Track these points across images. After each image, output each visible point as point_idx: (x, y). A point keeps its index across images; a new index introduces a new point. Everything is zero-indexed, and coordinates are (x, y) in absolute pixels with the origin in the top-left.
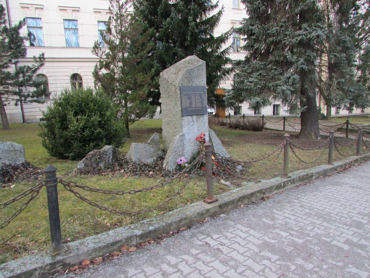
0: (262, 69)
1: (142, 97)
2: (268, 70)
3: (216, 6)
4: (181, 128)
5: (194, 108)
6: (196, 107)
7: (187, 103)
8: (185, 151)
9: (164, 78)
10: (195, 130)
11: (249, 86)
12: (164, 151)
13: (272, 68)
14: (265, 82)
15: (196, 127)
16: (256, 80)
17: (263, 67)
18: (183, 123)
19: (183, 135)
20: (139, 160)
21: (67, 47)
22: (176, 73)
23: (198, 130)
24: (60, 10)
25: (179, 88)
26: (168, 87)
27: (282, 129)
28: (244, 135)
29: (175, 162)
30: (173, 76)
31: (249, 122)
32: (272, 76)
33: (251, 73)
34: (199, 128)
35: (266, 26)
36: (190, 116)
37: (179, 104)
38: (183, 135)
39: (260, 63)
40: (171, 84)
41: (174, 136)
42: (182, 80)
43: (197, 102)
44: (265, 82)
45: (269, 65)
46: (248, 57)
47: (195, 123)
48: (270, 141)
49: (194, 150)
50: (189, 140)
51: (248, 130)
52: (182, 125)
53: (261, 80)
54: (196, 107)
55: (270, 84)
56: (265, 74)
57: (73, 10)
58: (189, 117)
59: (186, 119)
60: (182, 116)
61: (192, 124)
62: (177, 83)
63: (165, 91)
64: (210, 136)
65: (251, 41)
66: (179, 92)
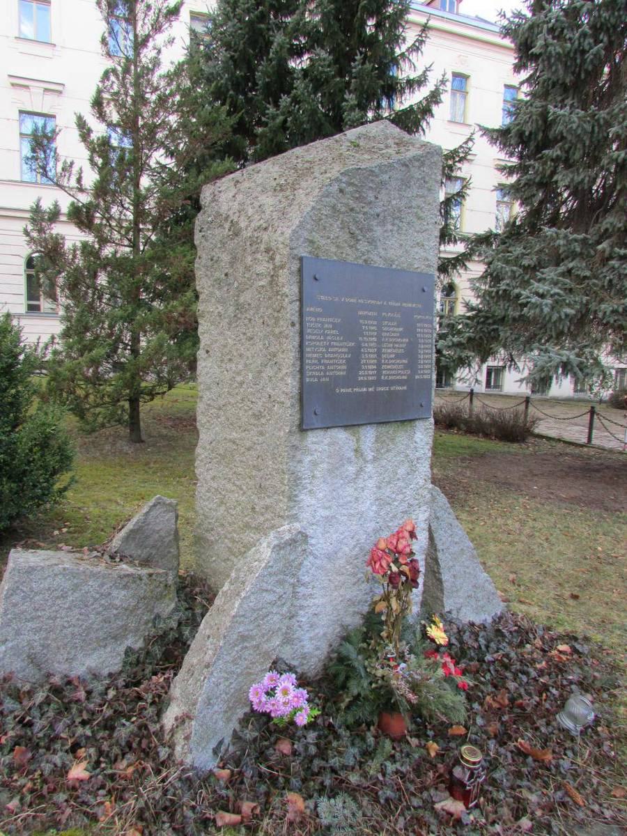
0: (573, 255)
1: (177, 322)
2: (597, 259)
3: (420, 82)
4: (292, 498)
5: (368, 384)
6: (378, 382)
7: (331, 357)
8: (303, 617)
9: (218, 214)
10: (367, 505)
11: (535, 306)
12: (195, 595)
13: (612, 251)
14: (585, 299)
15: (371, 484)
16: (556, 290)
17: (578, 250)
18: (304, 470)
19: (301, 539)
20: (33, 659)
21: (22, 182)
22: (282, 188)
23: (382, 502)
24: (13, 85)
25: (295, 266)
26: (234, 260)
27: (584, 440)
28: (483, 456)
29: (240, 697)
30: (268, 201)
31: (488, 414)
32: (610, 281)
33: (533, 269)
34: (387, 491)
35: (603, 114)
36: (346, 427)
37: (289, 357)
38: (301, 539)
39: (571, 237)
40: (254, 241)
41: (247, 526)
42: (317, 220)
43: (388, 351)
44: (585, 299)
45: (599, 243)
46: (518, 223)
47: (370, 468)
48: (577, 489)
49: (352, 602)
50: (330, 557)
51: (487, 435)
52: (296, 481)
53: (571, 290)
54: (378, 382)
55: (603, 306)
56: (588, 273)
57: (46, 90)
58: (341, 435)
59: (324, 444)
60: (303, 428)
61: (352, 469)
62: (282, 235)
63: (218, 281)
64: (431, 538)
65: (545, 163)
66: (291, 290)
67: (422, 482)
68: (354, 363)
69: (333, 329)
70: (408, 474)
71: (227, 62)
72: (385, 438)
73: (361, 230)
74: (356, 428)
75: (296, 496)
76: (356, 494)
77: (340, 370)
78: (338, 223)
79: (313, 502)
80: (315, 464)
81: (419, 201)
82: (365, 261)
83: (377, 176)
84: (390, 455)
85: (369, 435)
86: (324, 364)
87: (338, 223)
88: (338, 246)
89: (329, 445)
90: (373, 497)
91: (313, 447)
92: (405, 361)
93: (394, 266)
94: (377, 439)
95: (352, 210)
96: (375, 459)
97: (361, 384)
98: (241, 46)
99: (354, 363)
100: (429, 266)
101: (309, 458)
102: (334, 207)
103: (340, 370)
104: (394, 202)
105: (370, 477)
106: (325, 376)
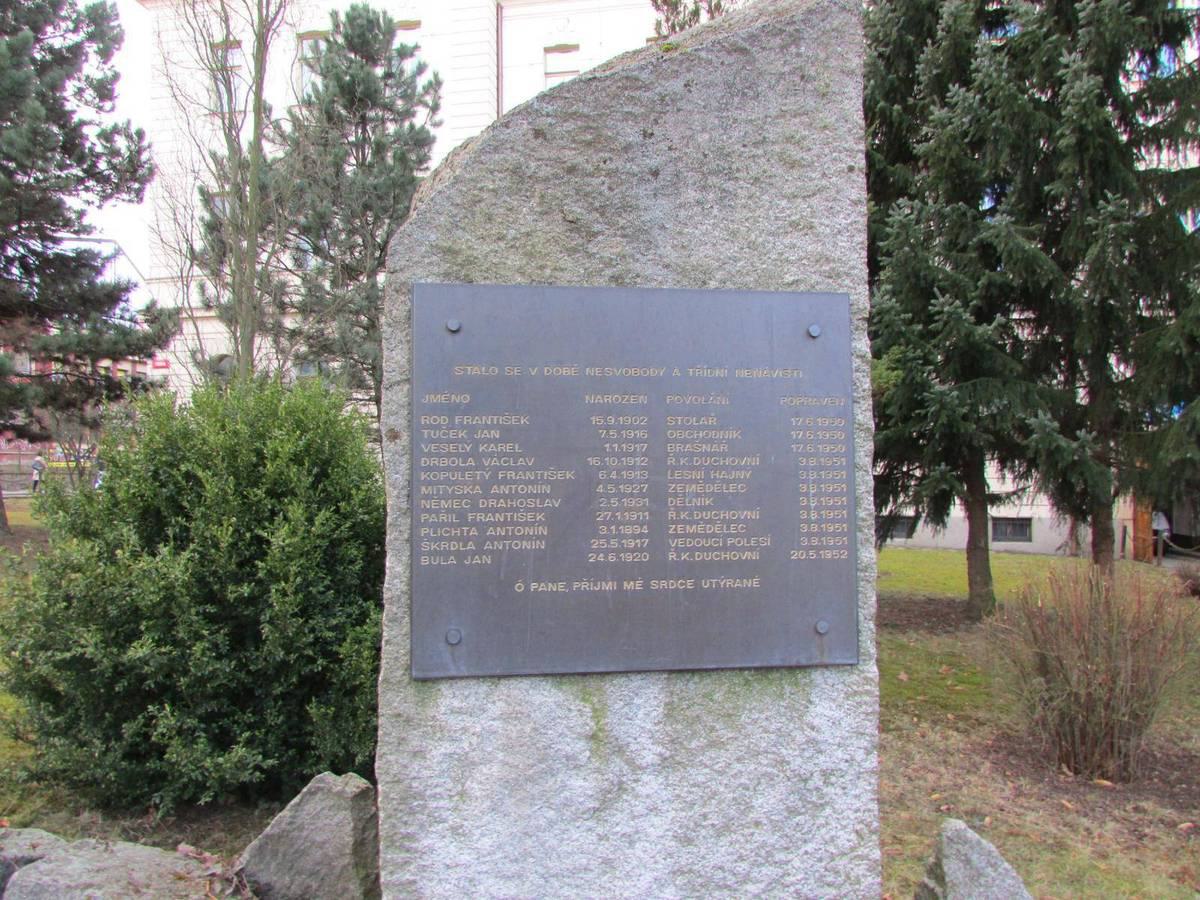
6: (658, 568)
36: (559, 677)
47: (650, 785)
54: (646, 571)
58: (544, 697)
61: (582, 786)
67: (846, 839)
68: (575, 513)
69: (501, 440)
70: (793, 811)
71: (874, 64)
72: (696, 710)
73: (602, 211)
74: (593, 683)
75: (409, 836)
76: (604, 849)
77: (528, 538)
78: (534, 202)
79: (465, 858)
80: (465, 764)
81: (794, 126)
82: (614, 278)
83: (646, 87)
84: (723, 757)
85: (640, 708)
86: (474, 523)
87: (534, 202)
88: (530, 255)
89: (505, 717)
90: (663, 866)
91: (455, 722)
92: (754, 515)
93: (713, 284)
94: (671, 713)
95: (572, 170)
96: (666, 764)
97: (597, 572)
98: (894, 35)
99: (575, 513)
100: (834, 275)
101: (446, 747)
102: (516, 171)
103: (528, 538)
104: (703, 138)
105: (653, 810)
106: (480, 552)
